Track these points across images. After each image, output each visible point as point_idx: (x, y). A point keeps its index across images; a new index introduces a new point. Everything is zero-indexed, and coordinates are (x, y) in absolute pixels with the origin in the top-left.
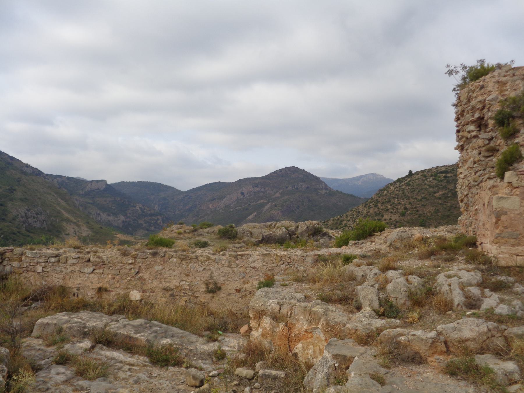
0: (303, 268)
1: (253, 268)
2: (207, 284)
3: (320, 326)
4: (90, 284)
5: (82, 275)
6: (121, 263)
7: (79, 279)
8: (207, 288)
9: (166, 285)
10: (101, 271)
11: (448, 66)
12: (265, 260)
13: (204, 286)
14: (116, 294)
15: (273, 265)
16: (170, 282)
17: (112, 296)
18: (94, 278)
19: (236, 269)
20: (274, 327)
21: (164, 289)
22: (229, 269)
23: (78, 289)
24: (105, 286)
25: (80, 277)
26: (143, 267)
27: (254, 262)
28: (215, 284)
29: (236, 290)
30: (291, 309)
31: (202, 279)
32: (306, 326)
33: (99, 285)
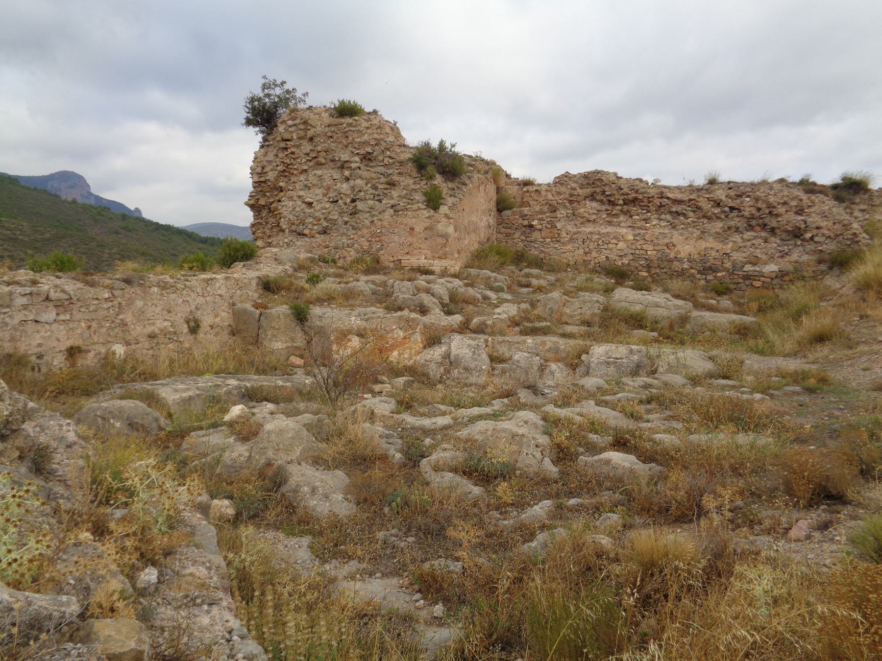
1: (220, 296)
2: (188, 322)
3: (418, 330)
4: (55, 343)
5: (39, 327)
6: (97, 299)
7: (38, 336)
9: (150, 329)
10: (68, 317)
11: (264, 77)
13: (186, 326)
14: (95, 355)
16: (154, 324)
17: (89, 360)
18: (60, 331)
21: (149, 336)
23: (40, 357)
24: (77, 344)
25: (38, 332)
26: (124, 303)
27: (219, 288)
33: (69, 343)
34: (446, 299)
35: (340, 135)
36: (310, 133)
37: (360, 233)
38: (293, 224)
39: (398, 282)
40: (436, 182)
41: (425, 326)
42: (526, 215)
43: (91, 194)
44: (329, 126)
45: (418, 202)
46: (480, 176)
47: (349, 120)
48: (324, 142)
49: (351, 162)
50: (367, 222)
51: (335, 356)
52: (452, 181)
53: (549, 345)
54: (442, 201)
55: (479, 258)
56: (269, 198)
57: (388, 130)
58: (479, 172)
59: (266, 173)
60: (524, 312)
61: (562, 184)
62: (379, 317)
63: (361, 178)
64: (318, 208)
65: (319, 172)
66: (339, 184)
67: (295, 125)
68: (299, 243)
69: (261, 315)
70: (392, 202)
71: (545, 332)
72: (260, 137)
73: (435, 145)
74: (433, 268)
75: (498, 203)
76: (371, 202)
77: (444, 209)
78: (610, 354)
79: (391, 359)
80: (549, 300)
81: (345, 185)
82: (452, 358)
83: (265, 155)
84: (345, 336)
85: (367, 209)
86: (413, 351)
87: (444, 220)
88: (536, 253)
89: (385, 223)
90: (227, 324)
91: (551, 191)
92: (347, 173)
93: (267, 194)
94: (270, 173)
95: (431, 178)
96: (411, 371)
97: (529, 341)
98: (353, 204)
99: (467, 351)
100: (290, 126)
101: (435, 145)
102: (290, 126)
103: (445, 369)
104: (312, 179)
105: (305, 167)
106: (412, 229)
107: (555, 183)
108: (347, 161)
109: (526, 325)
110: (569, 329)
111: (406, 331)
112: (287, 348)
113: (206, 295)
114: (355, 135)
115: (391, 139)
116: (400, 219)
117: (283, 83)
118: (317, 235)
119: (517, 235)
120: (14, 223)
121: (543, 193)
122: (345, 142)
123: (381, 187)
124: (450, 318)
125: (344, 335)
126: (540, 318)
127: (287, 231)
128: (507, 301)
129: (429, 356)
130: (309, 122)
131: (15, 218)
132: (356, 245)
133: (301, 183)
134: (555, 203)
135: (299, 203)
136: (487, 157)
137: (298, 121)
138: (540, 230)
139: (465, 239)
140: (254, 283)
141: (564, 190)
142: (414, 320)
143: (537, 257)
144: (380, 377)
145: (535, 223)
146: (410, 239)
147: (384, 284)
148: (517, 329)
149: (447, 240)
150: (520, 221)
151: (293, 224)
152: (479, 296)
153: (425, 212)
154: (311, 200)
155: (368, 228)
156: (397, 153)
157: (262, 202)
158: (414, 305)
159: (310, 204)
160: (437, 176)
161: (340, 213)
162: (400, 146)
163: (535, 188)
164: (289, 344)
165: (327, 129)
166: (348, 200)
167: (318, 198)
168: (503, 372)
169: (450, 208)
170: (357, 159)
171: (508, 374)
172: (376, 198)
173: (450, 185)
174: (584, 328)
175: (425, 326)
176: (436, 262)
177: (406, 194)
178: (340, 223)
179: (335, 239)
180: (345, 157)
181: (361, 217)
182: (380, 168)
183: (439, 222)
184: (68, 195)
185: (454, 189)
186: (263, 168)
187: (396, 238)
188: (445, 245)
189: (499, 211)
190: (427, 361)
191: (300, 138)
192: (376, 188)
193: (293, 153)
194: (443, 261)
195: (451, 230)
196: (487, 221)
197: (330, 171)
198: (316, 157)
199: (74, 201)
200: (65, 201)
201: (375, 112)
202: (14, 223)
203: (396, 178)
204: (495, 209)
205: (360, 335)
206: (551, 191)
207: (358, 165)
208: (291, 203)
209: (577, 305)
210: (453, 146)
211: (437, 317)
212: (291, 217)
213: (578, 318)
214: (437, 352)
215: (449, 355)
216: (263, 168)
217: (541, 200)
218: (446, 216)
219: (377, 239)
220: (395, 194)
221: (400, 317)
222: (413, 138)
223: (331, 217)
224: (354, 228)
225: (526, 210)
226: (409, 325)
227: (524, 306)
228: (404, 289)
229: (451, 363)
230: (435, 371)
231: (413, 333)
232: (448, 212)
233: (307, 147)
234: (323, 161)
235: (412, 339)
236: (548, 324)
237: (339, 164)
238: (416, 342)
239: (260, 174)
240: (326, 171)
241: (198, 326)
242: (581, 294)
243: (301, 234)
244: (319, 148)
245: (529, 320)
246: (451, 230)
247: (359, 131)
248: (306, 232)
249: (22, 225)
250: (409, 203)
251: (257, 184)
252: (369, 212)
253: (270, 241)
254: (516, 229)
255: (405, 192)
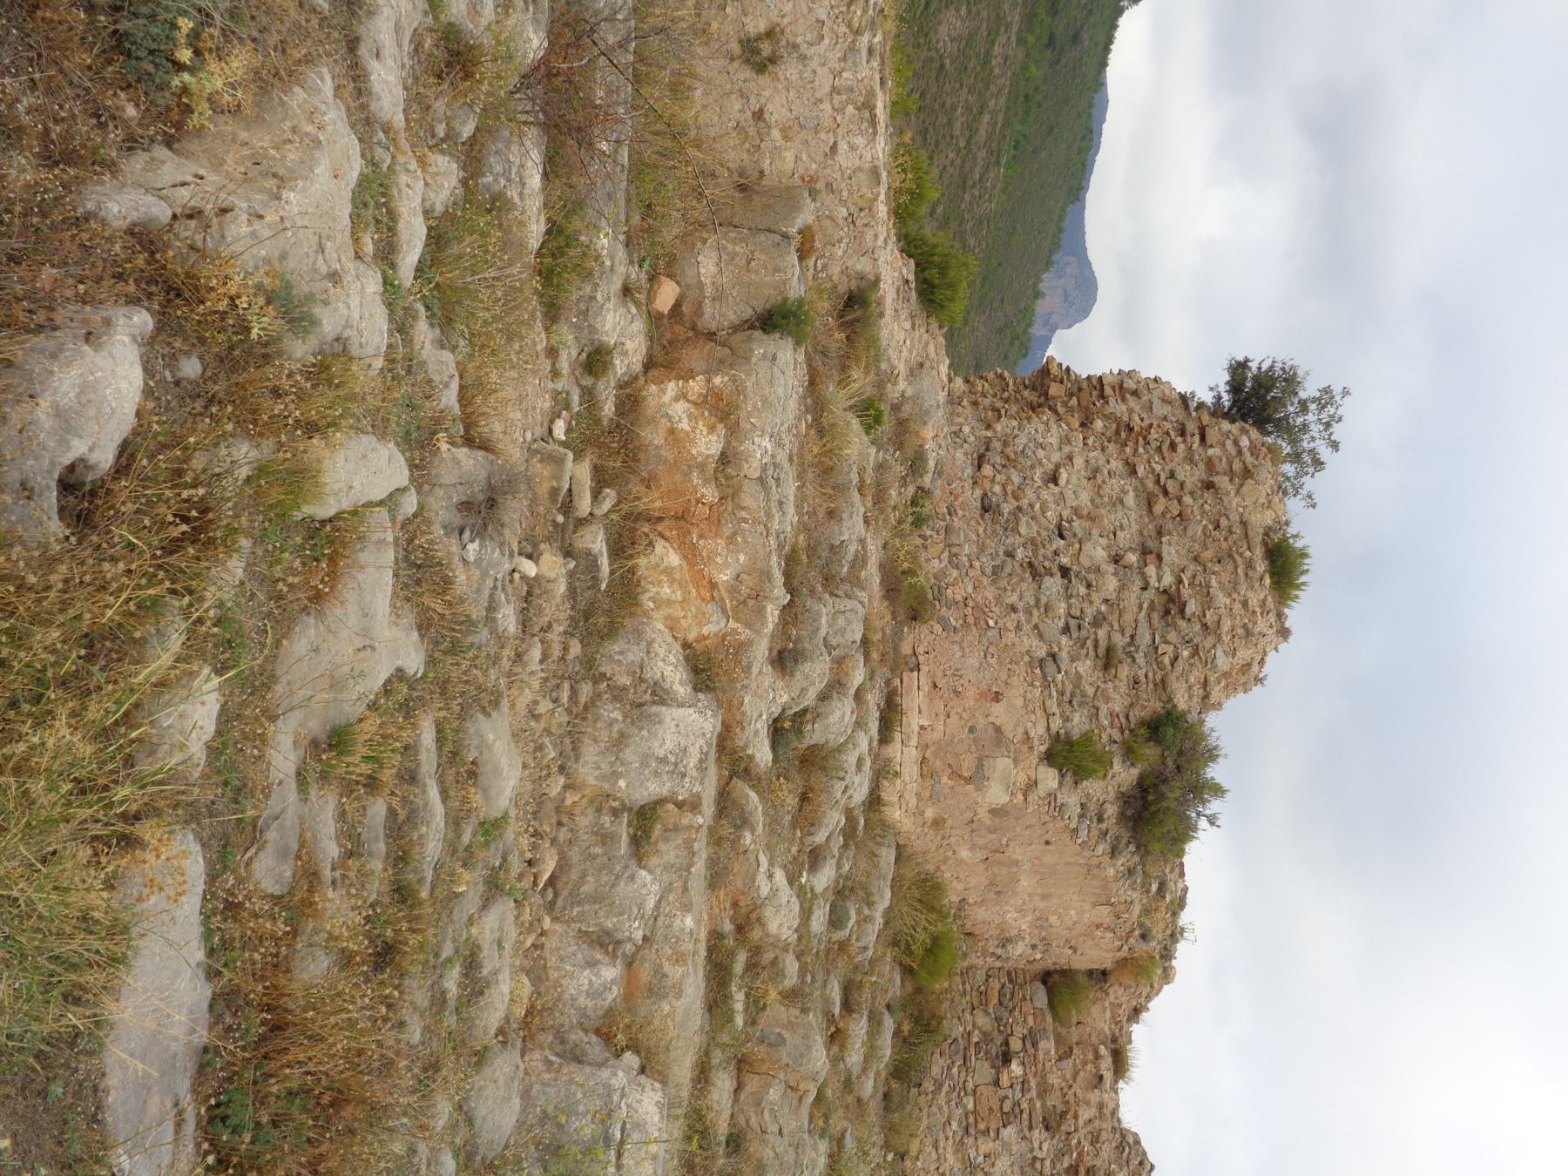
0: (840, 253)
1: (834, 148)
2: (769, 34)
3: (732, 624)
8: (759, 38)
11: (1346, 392)
12: (860, 174)
13: (762, 26)
15: (845, 194)
19: (826, 106)
20: (702, 467)
22: (827, 89)
27: (853, 148)
28: (773, 60)
29: (761, 111)
30: (756, 521)
31: (786, 21)
32: (724, 577)
34: (815, 734)
35: (1224, 545)
36: (1222, 481)
37: (985, 581)
38: (1005, 444)
39: (861, 611)
40: (1117, 766)
41: (742, 647)
42: (1035, 1045)
43: (1053, 330)
44: (1244, 524)
45: (1067, 720)
46: (1137, 909)
47: (1261, 566)
48: (1203, 513)
49: (1159, 567)
50: (1013, 598)
51: (672, 388)
52: (1122, 817)
53: (674, 972)
54: (1069, 779)
55: (924, 892)
56: (1065, 404)
57: (1244, 654)
58: (1146, 911)
59: (1124, 399)
60: (774, 962)
61: (1120, 1148)
62: (769, 516)
63: (1122, 588)
64: (1045, 494)
65: (1130, 500)
66: (1103, 541)
67: (1240, 452)
68: (959, 455)
69: (785, 236)
70: (1064, 656)
71: (717, 1003)
72: (1207, 398)
73: (1215, 772)
74: (897, 745)
75: (1066, 974)
76: (1061, 608)
77: (1049, 778)
78: (636, 1136)
79: (660, 546)
80: (806, 1036)
81: (1100, 554)
82: (655, 709)
83: (1166, 401)
84: (724, 418)
85: (1044, 600)
86: (677, 612)
87: (1022, 778)
88: (936, 1070)
89: (1011, 637)
90: (766, 165)
91: (1101, 1116)
92: (1132, 558)
93: (1074, 401)
94: (1124, 408)
95: (1129, 754)
96: (626, 590)
97: (689, 922)
98: (1055, 569)
99: (669, 745)
100: (1236, 443)
101: (1215, 772)
102: (1236, 443)
103: (624, 689)
104: (1114, 486)
105: (1141, 471)
106: (997, 697)
107: (1124, 1134)
108: (1160, 558)
109: (732, 955)
110: (723, 1083)
111: (733, 590)
112: (701, 286)
113: (837, 98)
114: (1226, 577)
115: (1223, 662)
116: (1021, 669)
117: (1335, 445)
118: (978, 492)
119: (983, 1021)
120: (994, 186)
121: (1094, 1096)
122: (1208, 554)
123: (1101, 633)
124: (762, 727)
125: (722, 410)
126: (756, 1005)
127: (989, 434)
128: (806, 914)
129: (661, 652)
130: (1250, 481)
131: (1004, 191)
132: (955, 573)
133: (1102, 462)
134: (1068, 1126)
135: (1056, 457)
136: (1185, 956)
137: (1249, 459)
138: (997, 1083)
139: (973, 848)
140: (863, 265)
141: (1104, 1155)
142: (760, 612)
143: (925, 1071)
144: (610, 495)
145: (1016, 1068)
146: (971, 692)
147: (855, 580)
148: (728, 927)
149: (968, 780)
150: (1020, 1031)
151: (1005, 444)
152: (820, 837)
153: (1041, 730)
154: (1062, 482)
155: (998, 599)
156: (1185, 675)
157: (1055, 390)
158: (798, 640)
159: (1054, 479)
160: (1135, 772)
161: (1033, 541)
162: (1205, 683)
163: (1108, 1076)
164: (709, 291)
165: (1235, 517)
166: (1065, 560)
167: (1069, 495)
168: (606, 839)
169: (1052, 796)
170: (1168, 579)
171: (598, 850)
172: (1073, 623)
173: (1111, 810)
174: (722, 1129)
175: (742, 647)
176: (912, 753)
177: (1084, 695)
178: (1010, 541)
179: (969, 531)
180: (1172, 552)
181: (1024, 586)
182: (1148, 637)
183: (1016, 761)
184: (1048, 282)
185: (1100, 820)
186: (1135, 393)
187: (973, 661)
188: (955, 774)
189: (1046, 977)
190: (649, 644)
191: (1209, 463)
192: (1098, 621)
193: (1173, 446)
194: (916, 769)
195: (996, 794)
196: (1020, 937)
197: (1135, 527)
198: (1166, 493)
199: (1038, 295)
200: (1038, 280)
201: (1284, 633)
202: (994, 186)
203: (1124, 671)
204: (1048, 964)
205: (725, 459)
206: (1101, 1116)
207: (1153, 582)
208: (1054, 441)
209: (791, 1125)
210: (1212, 821)
211: (763, 697)
212: (1022, 440)
213: (754, 1121)
214: (671, 671)
215: (663, 702)
216: (1135, 393)
217: (1077, 1088)
218: (1033, 784)
219: (971, 620)
220: (1085, 667)
221: (767, 575)
222: (1228, 725)
223: (1024, 519)
224: (997, 571)
225: (1047, 1045)
226: (747, 603)
227: (791, 966)
228: (841, 622)
229: (641, 705)
230: (620, 657)
231: (724, 611)
232: (1042, 790)
233: (1190, 476)
234: (1158, 509)
235: (710, 608)
236: (739, 1021)
237: (1150, 544)
238: (702, 619)
239: (1120, 388)
240: (1133, 516)
241: (761, 68)
242: (824, 1146)
243: (980, 461)
244: (1187, 499)
245: (752, 967)
246: (996, 794)
247: (1236, 584)
248: (987, 470)
249: (990, 201)
250: (1061, 693)
251: (1098, 384)
252: (1038, 601)
253: (965, 403)
254: (998, 1019)
255: (1090, 691)
